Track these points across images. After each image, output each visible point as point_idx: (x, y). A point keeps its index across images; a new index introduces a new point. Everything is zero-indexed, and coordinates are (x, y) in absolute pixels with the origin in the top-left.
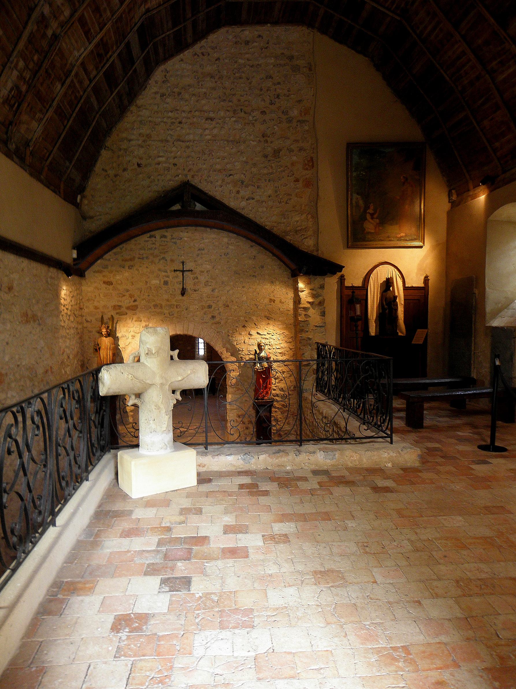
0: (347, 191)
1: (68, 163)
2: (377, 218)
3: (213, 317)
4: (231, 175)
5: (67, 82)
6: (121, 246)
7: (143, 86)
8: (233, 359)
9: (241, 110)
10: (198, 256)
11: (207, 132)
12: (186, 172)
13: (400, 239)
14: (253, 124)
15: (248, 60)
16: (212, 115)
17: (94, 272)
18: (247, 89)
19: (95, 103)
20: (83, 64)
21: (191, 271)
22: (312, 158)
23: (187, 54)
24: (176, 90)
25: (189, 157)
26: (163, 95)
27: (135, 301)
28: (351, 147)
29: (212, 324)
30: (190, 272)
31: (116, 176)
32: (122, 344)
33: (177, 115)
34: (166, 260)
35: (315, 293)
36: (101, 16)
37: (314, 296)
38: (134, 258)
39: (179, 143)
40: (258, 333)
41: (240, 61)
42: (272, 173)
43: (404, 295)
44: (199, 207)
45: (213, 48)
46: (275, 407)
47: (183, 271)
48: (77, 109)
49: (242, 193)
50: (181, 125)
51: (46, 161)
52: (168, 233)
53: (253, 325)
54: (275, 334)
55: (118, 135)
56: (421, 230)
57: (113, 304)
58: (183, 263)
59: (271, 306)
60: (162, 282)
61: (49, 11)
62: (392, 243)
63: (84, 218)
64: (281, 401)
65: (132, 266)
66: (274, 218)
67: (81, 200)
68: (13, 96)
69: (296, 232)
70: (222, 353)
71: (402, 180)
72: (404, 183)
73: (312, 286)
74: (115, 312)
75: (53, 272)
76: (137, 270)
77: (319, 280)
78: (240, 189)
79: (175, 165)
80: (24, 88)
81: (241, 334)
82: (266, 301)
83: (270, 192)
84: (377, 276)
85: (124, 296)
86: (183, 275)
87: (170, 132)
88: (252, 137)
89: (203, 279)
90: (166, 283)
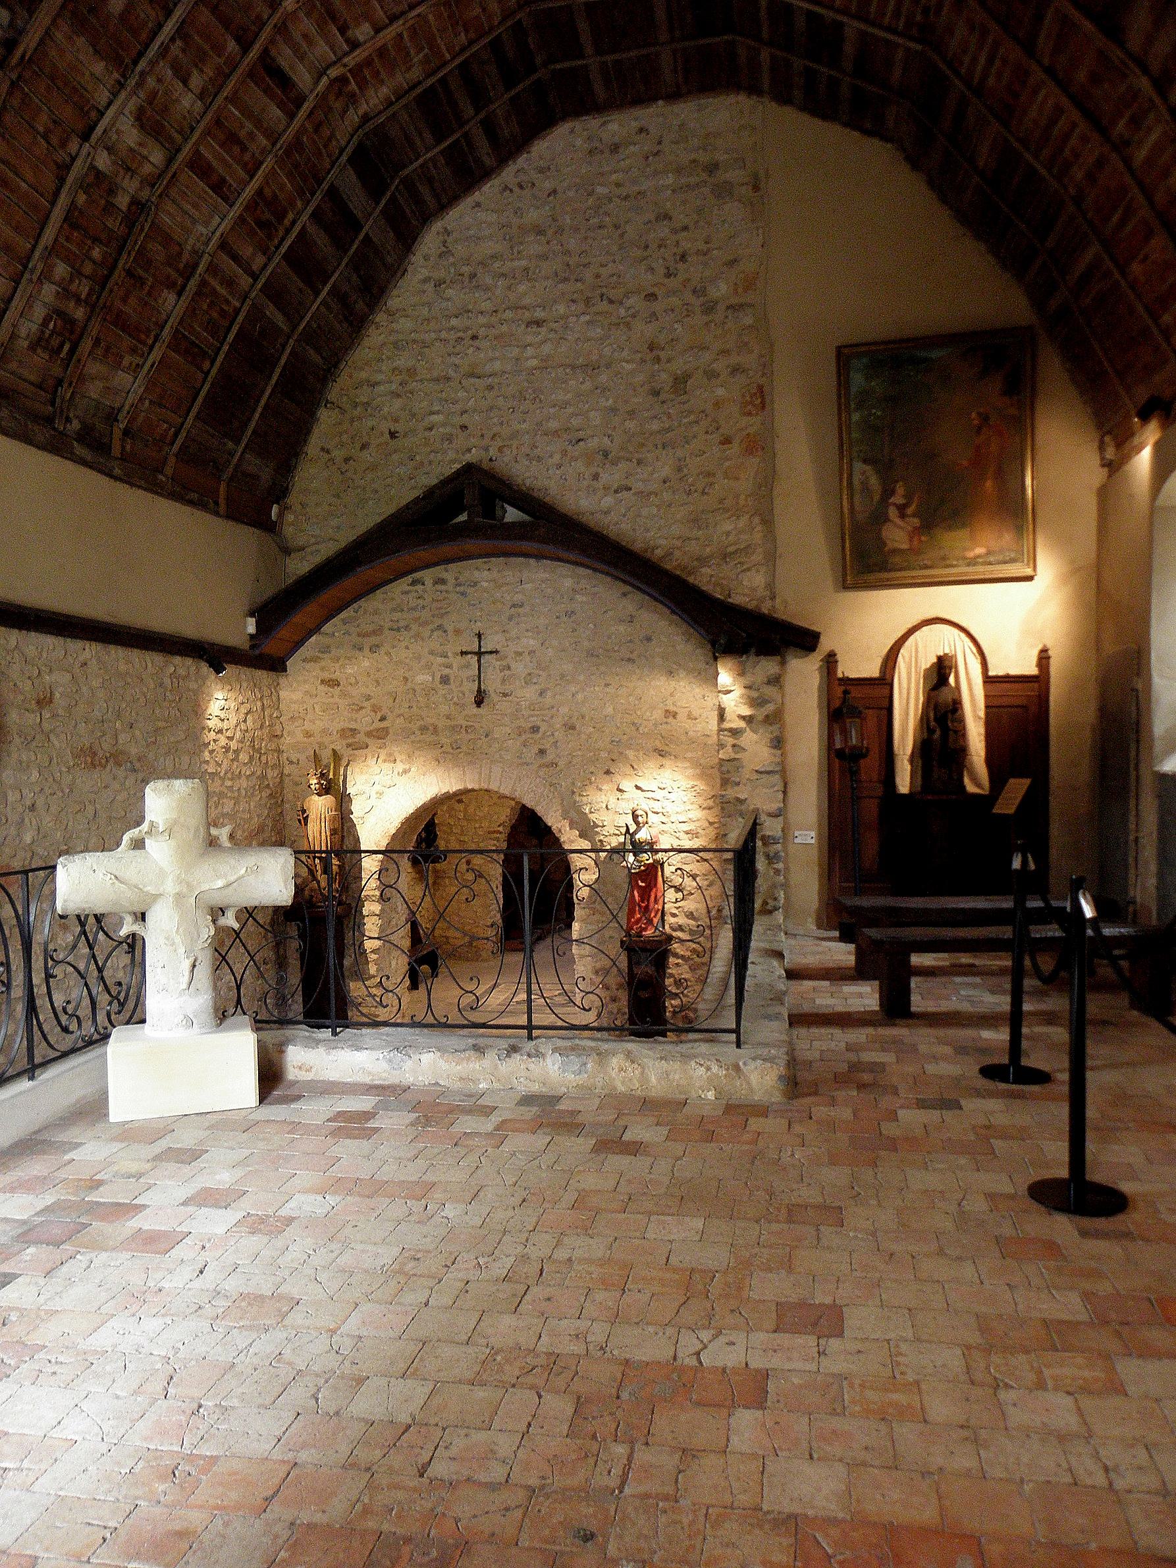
0: (841, 459)
1: (230, 445)
2: (914, 515)
3: (542, 752)
4: (579, 440)
5: (188, 288)
6: (355, 605)
7: (397, 270)
8: (586, 845)
9: (602, 296)
10: (510, 618)
11: (530, 351)
12: (486, 441)
13: (973, 562)
14: (628, 325)
15: (618, 185)
16: (539, 314)
17: (304, 661)
18: (615, 248)
19: (280, 320)
20: (223, 246)
21: (496, 652)
22: (761, 388)
23: (488, 191)
24: (466, 269)
25: (491, 408)
26: (438, 284)
27: (383, 719)
28: (844, 357)
29: (540, 766)
30: (494, 655)
31: (347, 460)
32: (357, 809)
33: (468, 323)
34: (445, 631)
35: (755, 694)
36: (244, 149)
37: (754, 702)
38: (381, 629)
39: (472, 380)
40: (637, 787)
41: (600, 190)
42: (669, 430)
43: (986, 696)
44: (512, 514)
45: (541, 171)
46: (676, 955)
47: (479, 654)
48: (231, 337)
49: (605, 477)
50: (477, 343)
51: (172, 443)
52: (450, 572)
53: (629, 770)
54: (676, 789)
55: (351, 377)
56: (1028, 540)
57: (339, 727)
58: (479, 636)
59: (669, 727)
60: (438, 679)
61: (109, 162)
62: (962, 570)
63: (287, 551)
64: (689, 941)
65: (377, 646)
66: (676, 530)
67: (281, 515)
68: (53, 332)
69: (725, 556)
70: (560, 831)
71: (976, 422)
72: (979, 431)
73: (748, 679)
74: (344, 742)
75: (182, 665)
76: (388, 654)
77: (768, 666)
78: (600, 470)
79: (464, 427)
80: (79, 314)
81: (601, 790)
82: (658, 715)
83: (666, 471)
84: (917, 651)
85: (362, 708)
86: (479, 661)
87: (454, 359)
88: (625, 354)
89: (519, 668)
90: (445, 680)
